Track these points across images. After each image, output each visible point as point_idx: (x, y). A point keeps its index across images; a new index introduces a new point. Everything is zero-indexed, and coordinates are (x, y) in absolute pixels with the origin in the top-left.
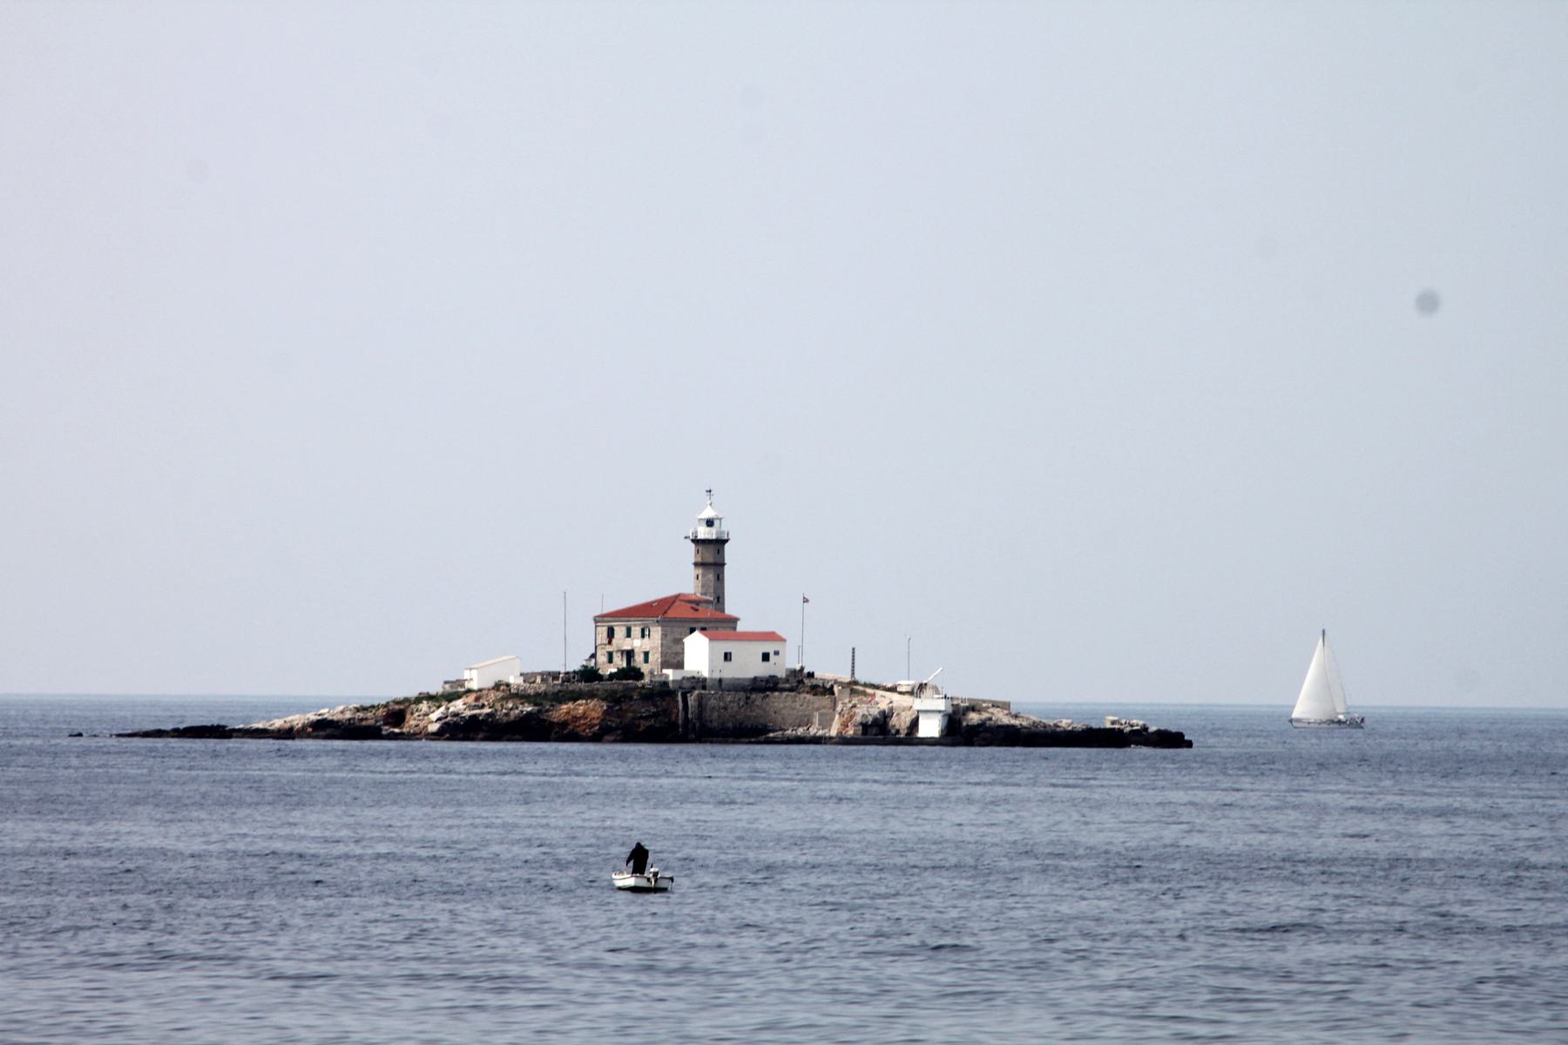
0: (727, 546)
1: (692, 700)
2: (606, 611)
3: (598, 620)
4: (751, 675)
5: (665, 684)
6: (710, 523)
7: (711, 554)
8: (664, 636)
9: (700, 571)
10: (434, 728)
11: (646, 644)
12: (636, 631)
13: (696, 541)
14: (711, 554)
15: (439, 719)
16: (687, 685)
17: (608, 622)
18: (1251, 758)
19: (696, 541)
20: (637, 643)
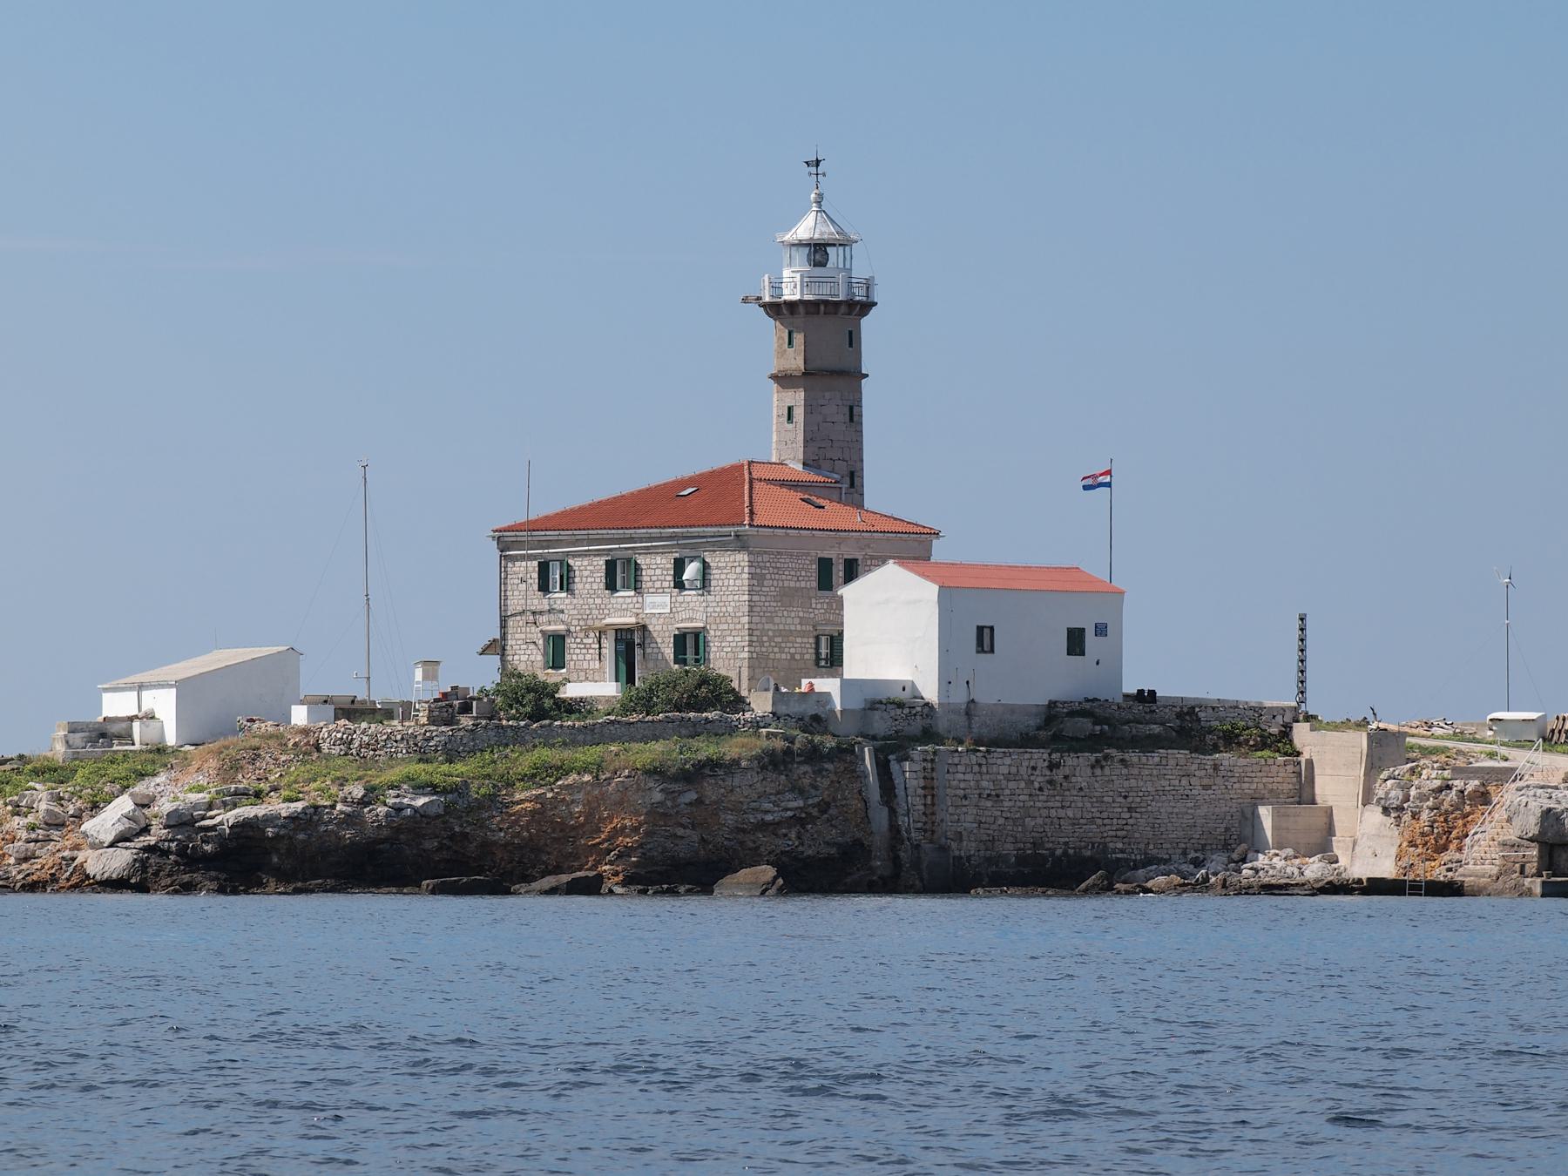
0: (867, 323)
1: (908, 773)
2: (543, 508)
3: (507, 542)
4: (1039, 697)
5: (817, 721)
6: (818, 251)
7: (826, 336)
8: (757, 579)
9: (797, 398)
10: (118, 861)
11: (712, 606)
12: (657, 567)
13: (777, 309)
14: (826, 336)
15: (122, 839)
16: (881, 724)
17: (540, 547)
18: (826, 866)
19: (777, 309)
20: (659, 608)
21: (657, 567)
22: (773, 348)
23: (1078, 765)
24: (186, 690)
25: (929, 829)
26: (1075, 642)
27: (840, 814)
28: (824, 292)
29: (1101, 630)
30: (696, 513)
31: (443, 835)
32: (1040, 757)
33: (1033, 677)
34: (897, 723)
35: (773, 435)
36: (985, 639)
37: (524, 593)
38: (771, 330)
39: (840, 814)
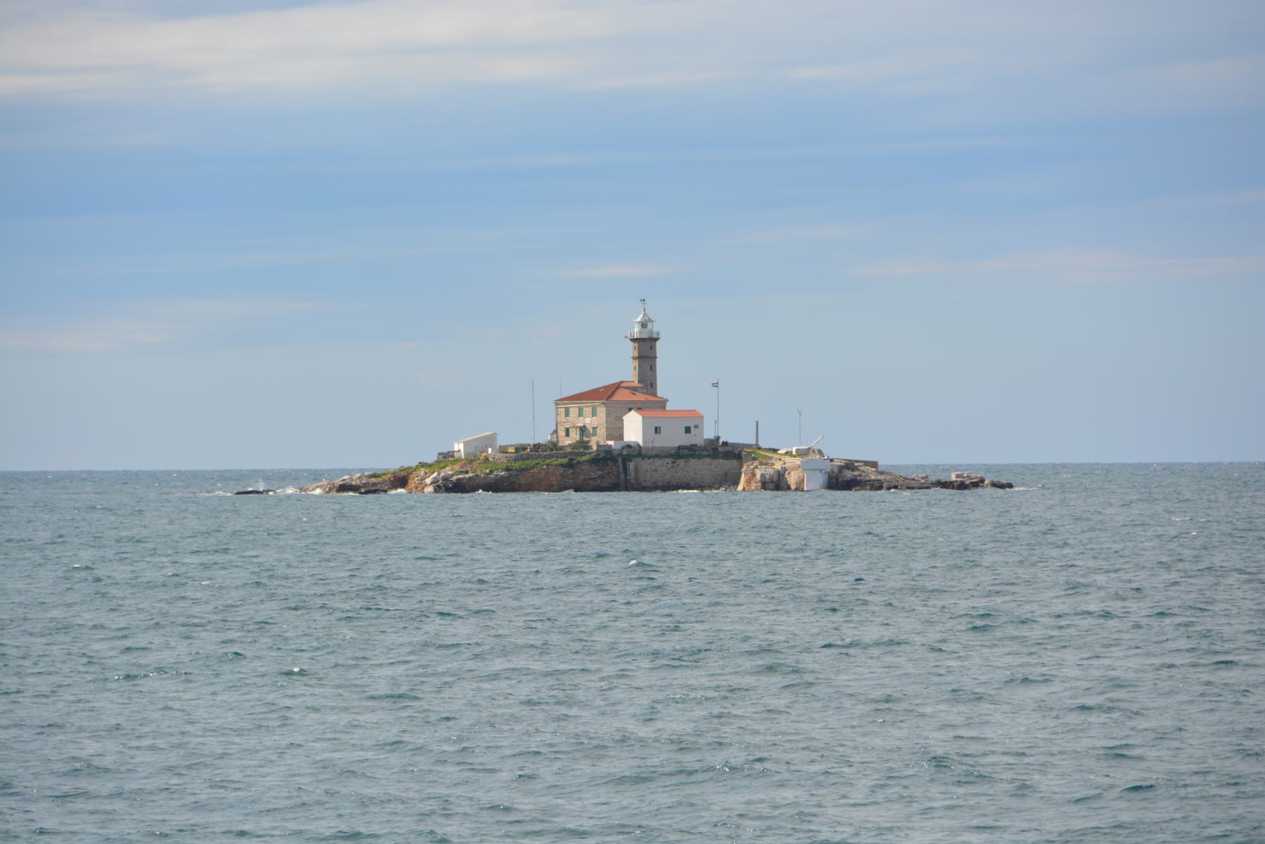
1: (631, 466)
2: (564, 396)
3: (559, 402)
7: (646, 348)
8: (608, 414)
13: (633, 340)
14: (646, 348)
19: (633, 340)
21: (587, 410)
22: (630, 350)
23: (681, 462)
24: (466, 444)
25: (637, 478)
26: (688, 430)
27: (610, 471)
28: (644, 336)
29: (696, 427)
30: (606, 394)
31: (525, 472)
32: (669, 460)
33: (674, 438)
34: (633, 453)
35: (628, 372)
36: (657, 430)
37: (562, 418)
38: (631, 344)
39: (610, 471)
